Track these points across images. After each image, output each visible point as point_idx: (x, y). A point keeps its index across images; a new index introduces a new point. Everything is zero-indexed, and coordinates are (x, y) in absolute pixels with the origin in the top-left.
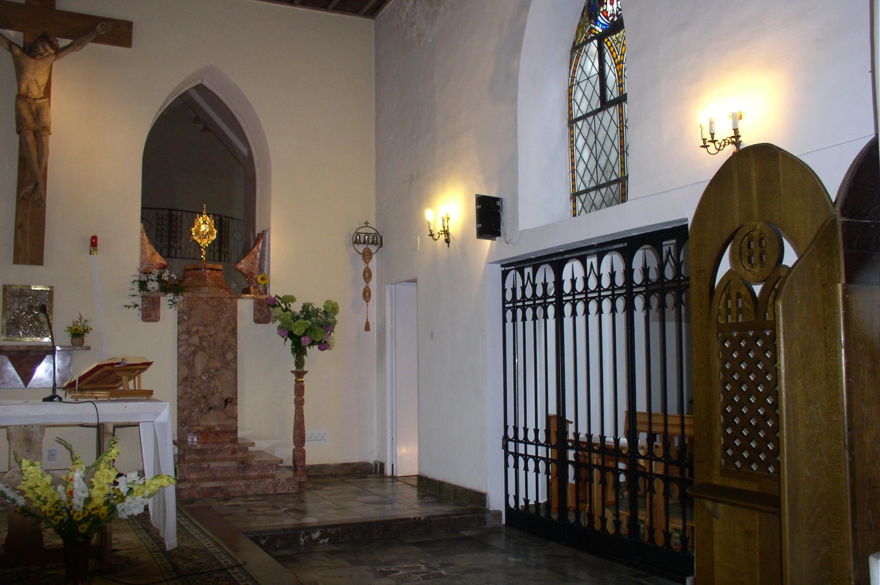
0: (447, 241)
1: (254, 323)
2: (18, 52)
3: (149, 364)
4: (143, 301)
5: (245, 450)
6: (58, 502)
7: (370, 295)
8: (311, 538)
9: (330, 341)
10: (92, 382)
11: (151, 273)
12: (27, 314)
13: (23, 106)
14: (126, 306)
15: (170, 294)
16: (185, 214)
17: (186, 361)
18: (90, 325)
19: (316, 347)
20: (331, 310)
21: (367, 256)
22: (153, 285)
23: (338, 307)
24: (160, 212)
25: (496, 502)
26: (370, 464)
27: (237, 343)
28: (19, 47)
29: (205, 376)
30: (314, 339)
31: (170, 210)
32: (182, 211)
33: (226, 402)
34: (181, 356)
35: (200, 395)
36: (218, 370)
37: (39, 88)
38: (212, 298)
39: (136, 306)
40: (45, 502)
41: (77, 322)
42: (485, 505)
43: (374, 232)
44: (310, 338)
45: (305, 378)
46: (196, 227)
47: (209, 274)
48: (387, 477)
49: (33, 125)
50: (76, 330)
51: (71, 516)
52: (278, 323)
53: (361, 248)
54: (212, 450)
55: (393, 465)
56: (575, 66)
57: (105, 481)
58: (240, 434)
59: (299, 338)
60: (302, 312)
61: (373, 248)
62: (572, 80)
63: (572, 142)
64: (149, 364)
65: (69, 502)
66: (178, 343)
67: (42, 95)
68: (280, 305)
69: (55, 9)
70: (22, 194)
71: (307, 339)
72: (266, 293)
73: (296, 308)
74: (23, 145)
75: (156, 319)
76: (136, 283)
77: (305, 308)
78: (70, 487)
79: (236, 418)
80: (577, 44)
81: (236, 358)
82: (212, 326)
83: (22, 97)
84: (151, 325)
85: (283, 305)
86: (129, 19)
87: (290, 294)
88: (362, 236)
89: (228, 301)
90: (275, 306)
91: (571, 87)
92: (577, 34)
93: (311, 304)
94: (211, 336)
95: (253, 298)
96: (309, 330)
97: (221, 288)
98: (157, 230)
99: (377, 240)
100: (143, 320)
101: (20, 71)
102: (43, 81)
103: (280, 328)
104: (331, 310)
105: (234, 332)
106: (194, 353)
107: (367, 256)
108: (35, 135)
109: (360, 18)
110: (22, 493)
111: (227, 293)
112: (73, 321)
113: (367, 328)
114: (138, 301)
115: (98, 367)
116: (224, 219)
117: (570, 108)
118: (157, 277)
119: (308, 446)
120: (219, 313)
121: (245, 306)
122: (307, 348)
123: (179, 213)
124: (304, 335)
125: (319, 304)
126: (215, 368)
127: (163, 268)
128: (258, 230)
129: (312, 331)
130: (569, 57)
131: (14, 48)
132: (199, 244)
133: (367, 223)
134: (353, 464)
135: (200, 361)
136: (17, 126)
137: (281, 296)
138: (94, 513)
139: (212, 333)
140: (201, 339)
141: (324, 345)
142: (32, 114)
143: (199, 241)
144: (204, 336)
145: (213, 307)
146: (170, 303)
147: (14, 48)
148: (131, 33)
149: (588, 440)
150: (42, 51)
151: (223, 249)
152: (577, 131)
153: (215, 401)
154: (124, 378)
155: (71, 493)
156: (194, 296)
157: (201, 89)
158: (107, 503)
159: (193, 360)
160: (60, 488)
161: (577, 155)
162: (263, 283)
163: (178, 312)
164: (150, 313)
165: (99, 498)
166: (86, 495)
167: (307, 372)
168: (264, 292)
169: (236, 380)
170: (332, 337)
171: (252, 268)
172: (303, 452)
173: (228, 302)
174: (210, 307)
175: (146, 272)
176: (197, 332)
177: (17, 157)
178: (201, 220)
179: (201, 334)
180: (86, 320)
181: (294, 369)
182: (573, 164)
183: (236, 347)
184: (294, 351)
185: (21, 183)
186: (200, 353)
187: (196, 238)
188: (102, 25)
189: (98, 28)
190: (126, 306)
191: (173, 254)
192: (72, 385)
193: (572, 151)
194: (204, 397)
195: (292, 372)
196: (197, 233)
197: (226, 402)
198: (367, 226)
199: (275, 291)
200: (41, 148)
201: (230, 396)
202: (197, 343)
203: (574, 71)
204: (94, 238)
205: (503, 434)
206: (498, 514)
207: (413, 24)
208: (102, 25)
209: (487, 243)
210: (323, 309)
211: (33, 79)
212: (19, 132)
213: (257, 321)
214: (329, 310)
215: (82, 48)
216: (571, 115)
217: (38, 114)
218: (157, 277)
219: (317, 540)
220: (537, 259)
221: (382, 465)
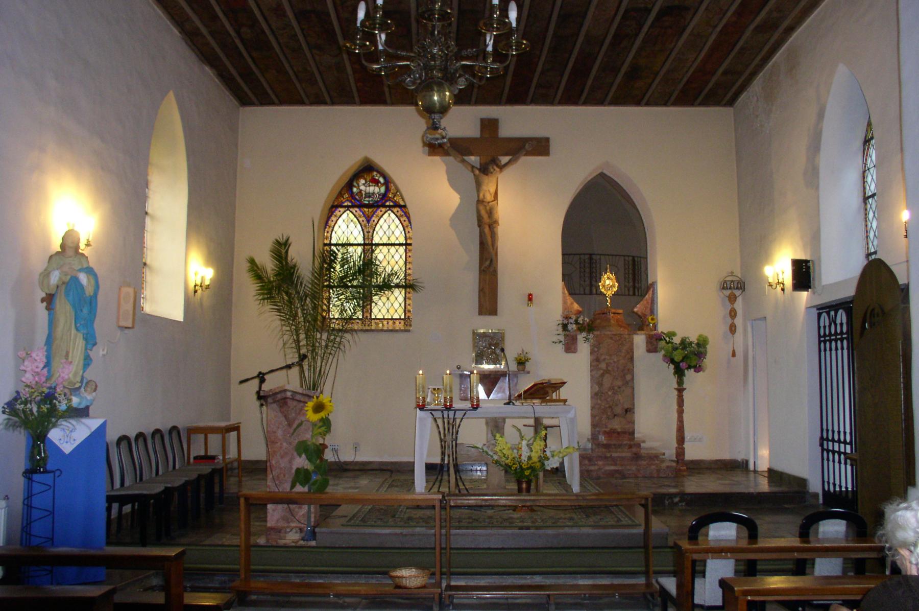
0: (783, 290)
2: (477, 172)
3: (564, 383)
4: (565, 338)
5: (638, 445)
6: (514, 458)
7: (735, 329)
8: (673, 501)
9: (703, 365)
10: (531, 394)
11: (570, 318)
12: (488, 349)
13: (481, 208)
16: (602, 257)
17: (597, 380)
18: (529, 356)
19: (693, 370)
20: (702, 343)
21: (732, 299)
22: (572, 327)
24: (582, 256)
25: (815, 486)
26: (738, 461)
28: (477, 168)
31: (591, 255)
32: (601, 255)
33: (626, 411)
35: (607, 406)
37: (491, 194)
38: (615, 335)
39: (561, 342)
40: (507, 458)
42: (805, 489)
43: (739, 279)
44: (686, 363)
45: (685, 393)
46: (602, 282)
48: (750, 471)
49: (488, 221)
50: (520, 359)
51: (521, 466)
52: (663, 352)
53: (728, 292)
54: (615, 445)
55: (755, 462)
56: (867, 155)
57: (539, 448)
58: (636, 435)
59: (679, 363)
60: (681, 344)
61: (737, 293)
62: (865, 166)
63: (866, 214)
64: (564, 383)
65: (520, 458)
67: (493, 199)
68: (665, 339)
69: (498, 138)
70: (482, 268)
72: (655, 330)
73: (677, 340)
74: (482, 235)
76: (561, 326)
78: (520, 452)
79: (633, 423)
80: (867, 139)
81: (633, 379)
83: (480, 202)
84: (571, 356)
85: (667, 339)
86: (548, 136)
87: (671, 330)
88: (728, 283)
89: (627, 337)
90: (661, 339)
91: (864, 172)
92: (867, 131)
93: (688, 338)
94: (614, 362)
95: (645, 334)
96: (685, 358)
98: (580, 272)
99: (741, 286)
101: (478, 185)
102: (492, 190)
103: (665, 356)
104: (702, 343)
105: (632, 359)
107: (732, 299)
108: (489, 227)
109: (721, 109)
110: (496, 453)
111: (626, 330)
113: (734, 355)
114: (562, 338)
115: (535, 385)
116: (636, 259)
117: (864, 188)
119: (686, 445)
121: (640, 340)
122: (686, 371)
124: (682, 361)
125: (694, 338)
127: (579, 313)
128: (650, 282)
130: (862, 149)
131: (475, 169)
132: (605, 295)
133: (732, 273)
134: (724, 460)
135: (607, 381)
136: (478, 223)
137: (665, 332)
138: (532, 465)
139: (615, 360)
140: (608, 365)
141: (698, 369)
142: (487, 212)
143: (605, 292)
146: (585, 339)
147: (475, 169)
148: (548, 146)
149: (184, 319)
150: (492, 170)
151: (636, 285)
152: (869, 206)
153: (618, 410)
154: (550, 391)
155: (521, 455)
157: (602, 175)
158: (540, 461)
159: (602, 380)
160: (515, 451)
161: (869, 225)
162: (653, 322)
164: (570, 346)
165: (535, 457)
166: (529, 454)
167: (685, 389)
168: (654, 329)
169: (633, 395)
172: (683, 449)
175: (567, 317)
176: (604, 359)
177: (478, 243)
178: (606, 276)
179: (607, 361)
181: (676, 386)
182: (867, 232)
183: (633, 370)
184: (675, 373)
185: (482, 260)
186: (607, 375)
187: (603, 290)
189: (527, 146)
192: (520, 396)
193: (866, 221)
194: (610, 407)
195: (675, 389)
196: (604, 286)
197: (626, 411)
198: (732, 275)
199: (662, 328)
200: (494, 235)
201: (629, 406)
202: (605, 368)
203: (866, 160)
205: (820, 435)
206: (816, 495)
207: (757, 116)
209: (804, 295)
210: (696, 342)
211: (487, 189)
212: (479, 226)
213: (649, 351)
214: (701, 343)
216: (865, 193)
217: (490, 213)
219: (677, 504)
220: (837, 305)
221: (747, 462)
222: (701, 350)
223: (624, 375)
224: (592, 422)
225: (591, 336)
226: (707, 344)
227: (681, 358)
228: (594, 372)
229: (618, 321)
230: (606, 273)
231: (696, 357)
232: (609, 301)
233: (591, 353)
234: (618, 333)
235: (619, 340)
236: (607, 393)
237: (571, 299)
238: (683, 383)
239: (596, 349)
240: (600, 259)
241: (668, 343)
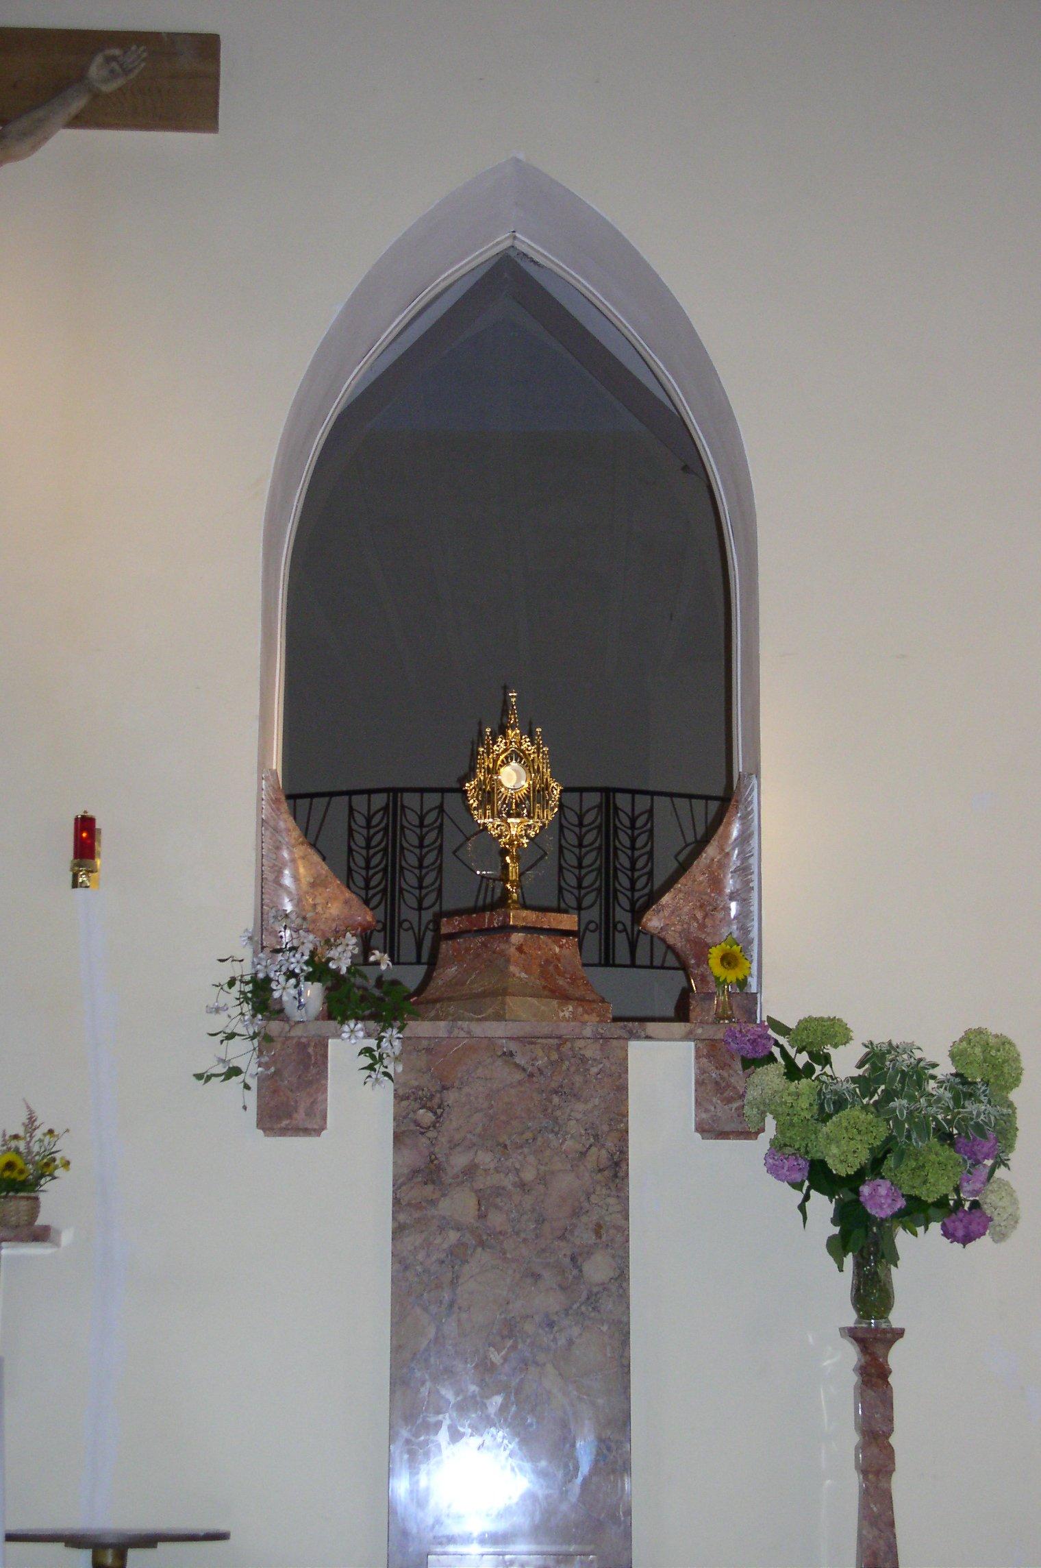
1: (698, 1135)
9: (992, 1201)
14: (199, 1077)
15: (352, 1023)
16: (661, 803)
18: (65, 1148)
23: (1017, 1059)
27: (627, 1219)
29: (499, 1351)
30: (916, 1192)
31: (608, 793)
34: (406, 1268)
36: (551, 1325)
39: (234, 1071)
41: (16, 1137)
45: (897, 1357)
47: (520, 949)
66: (394, 1218)
71: (883, 1191)
75: (313, 1126)
77: (875, 1058)
81: (622, 1276)
82: (526, 1150)
87: (821, 1010)
94: (523, 1186)
97: (565, 998)
100: (264, 1130)
103: (778, 1147)
106: (458, 1255)
112: (4, 1135)
114: (243, 1053)
118: (307, 963)
120: (556, 1099)
122: (902, 1238)
123: (642, 802)
125: (948, 1053)
126: (537, 1318)
129: (901, 1156)
137: (792, 1024)
139: (529, 1175)
140: (486, 1200)
144: (499, 1191)
145: (531, 1075)
156: (456, 1032)
163: (396, 1096)
167: (900, 1333)
170: (1004, 1184)
171: (702, 927)
173: (588, 1053)
174: (519, 1076)
176: (470, 1171)
179: (480, 1183)
180: (51, 1132)
181: (850, 1317)
183: (624, 1231)
188: (109, 59)
189: (96, 70)
190: (199, 1077)
191: (622, 953)
204: (85, 827)
208: (109, 59)
213: (709, 1129)
215: (34, 148)
218: (307, 963)
225: (393, 1040)
226: (1016, 1081)
227: (864, 1157)
228: (413, 1240)
229: (549, 968)
230: (502, 730)
231: (946, 1152)
234: (545, 1028)
239: (426, 1117)
240: (651, 812)
241: (793, 1072)
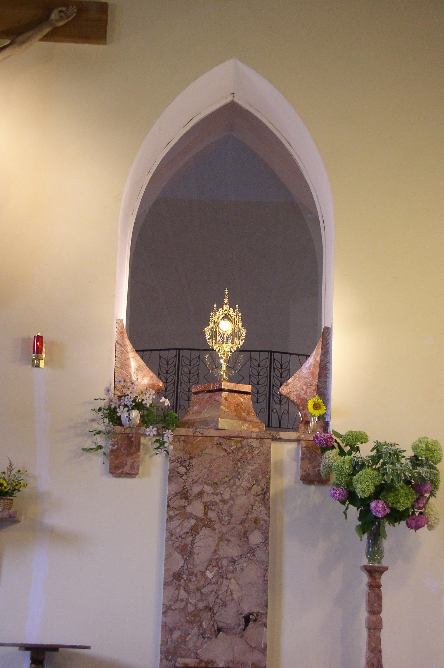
19: (403, 523)
35: (201, 605)
39: (100, 447)
45: (384, 579)
89: (255, 443)
137: (343, 433)
139: (226, 497)
140: (207, 506)
159: (193, 542)
176: (201, 494)
179: (206, 499)
181: (365, 562)
184: (363, 529)
194: (208, 608)
196: (214, 335)
222: (423, 471)
223: (245, 533)
224: (164, 643)
225: (168, 435)
228: (176, 523)
230: (220, 306)
232: (224, 366)
233: (170, 479)
235: (238, 449)
236: (203, 573)
237: (139, 358)
238: (381, 553)
239: (182, 470)
